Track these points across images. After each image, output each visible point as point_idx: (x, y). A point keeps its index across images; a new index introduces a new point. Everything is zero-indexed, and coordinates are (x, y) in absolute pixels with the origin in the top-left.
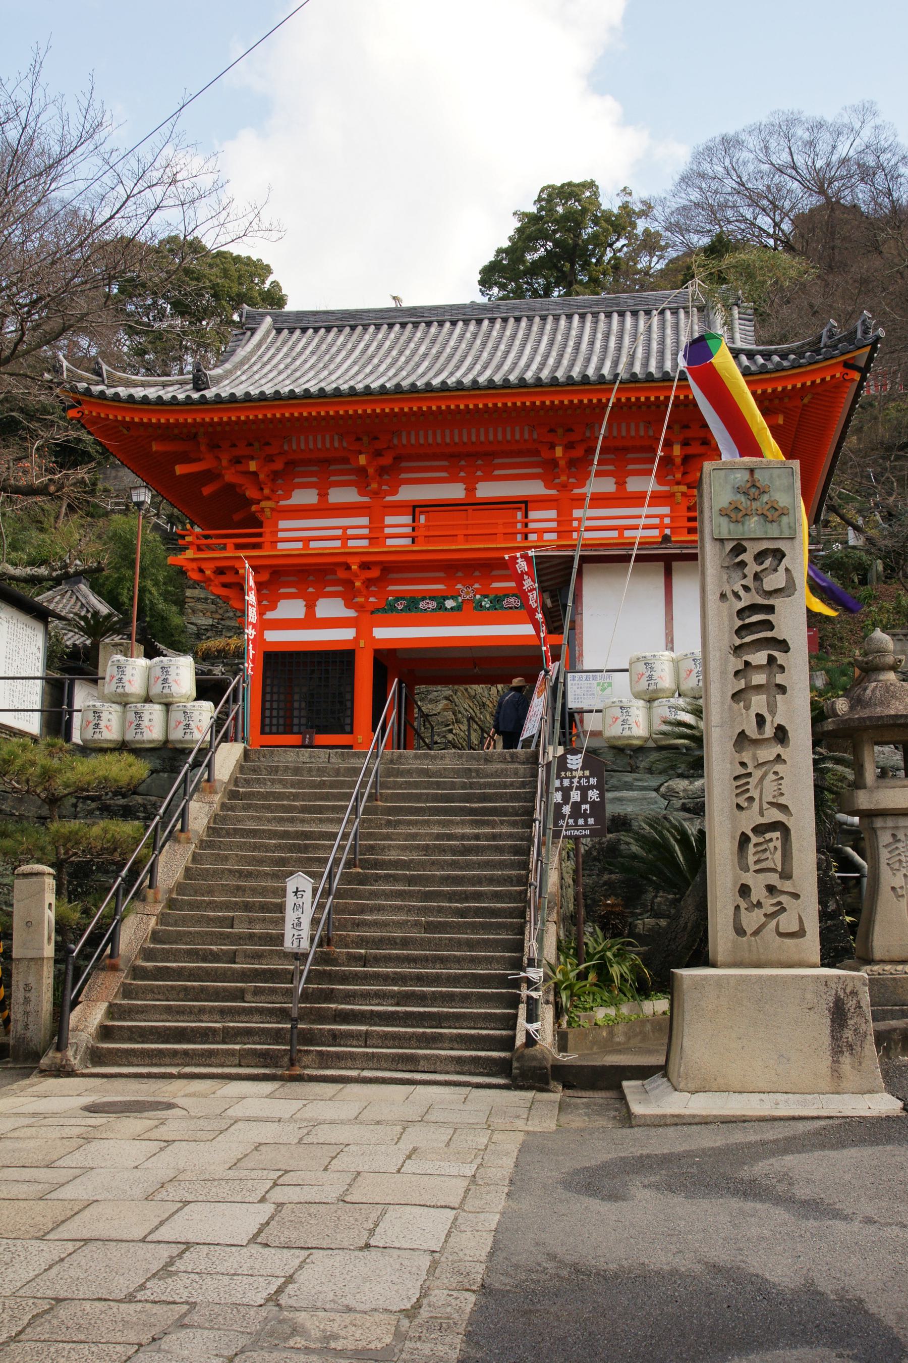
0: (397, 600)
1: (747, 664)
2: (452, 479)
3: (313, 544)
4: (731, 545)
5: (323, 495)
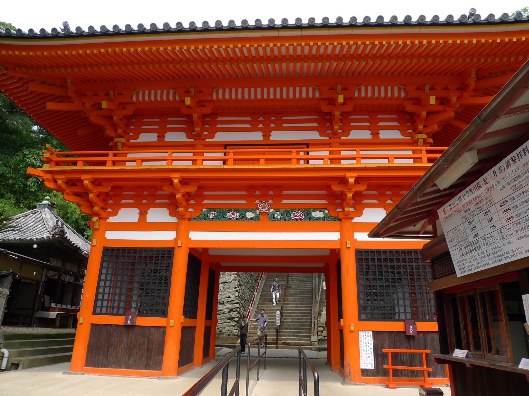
0: (209, 211)
5: (161, 137)
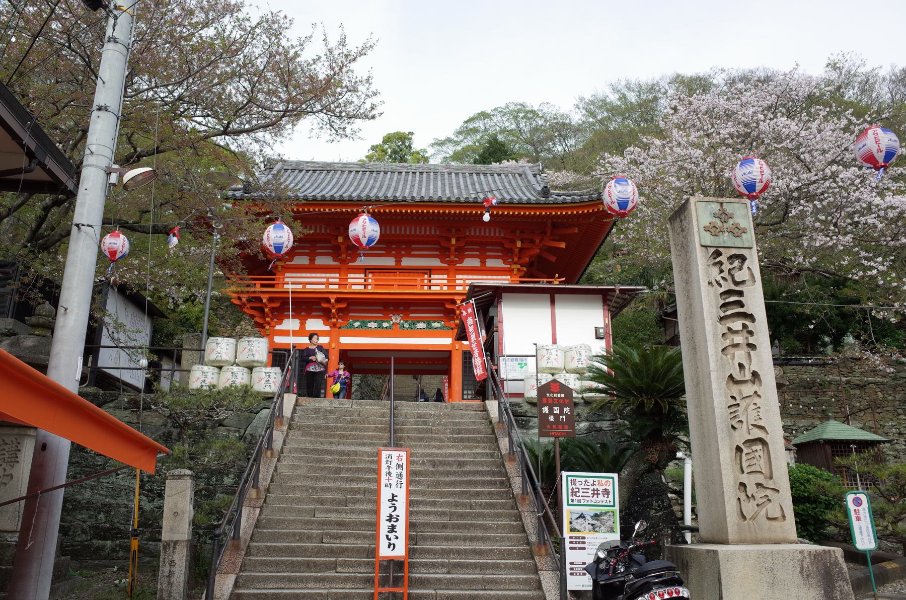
1: (729, 329)
2: (388, 255)
3: (308, 286)
4: (713, 250)
5: (312, 260)
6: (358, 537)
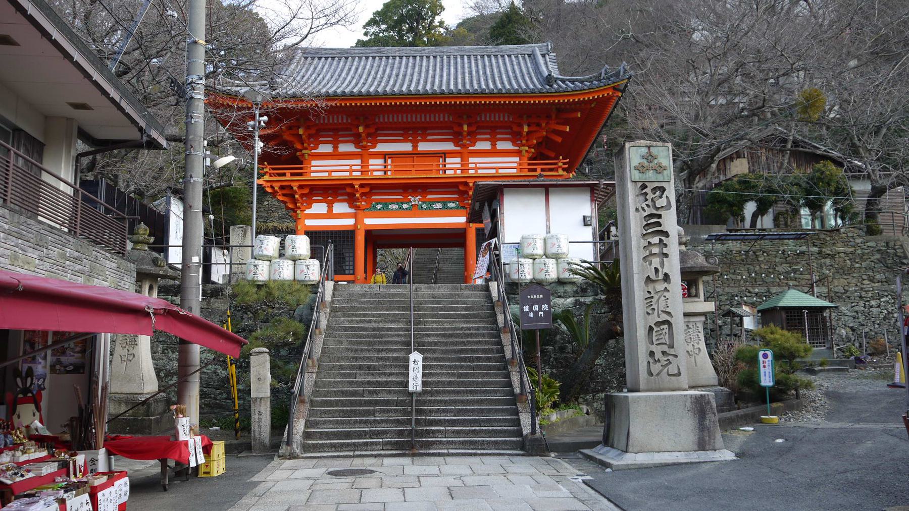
2: (405, 140)
3: (333, 174)
4: (640, 184)
6: (389, 392)
